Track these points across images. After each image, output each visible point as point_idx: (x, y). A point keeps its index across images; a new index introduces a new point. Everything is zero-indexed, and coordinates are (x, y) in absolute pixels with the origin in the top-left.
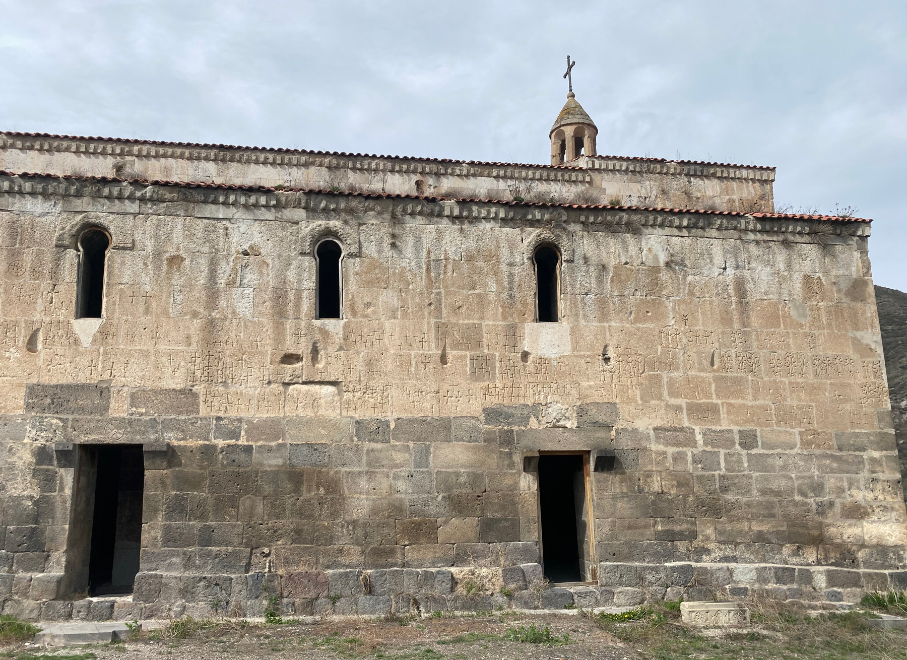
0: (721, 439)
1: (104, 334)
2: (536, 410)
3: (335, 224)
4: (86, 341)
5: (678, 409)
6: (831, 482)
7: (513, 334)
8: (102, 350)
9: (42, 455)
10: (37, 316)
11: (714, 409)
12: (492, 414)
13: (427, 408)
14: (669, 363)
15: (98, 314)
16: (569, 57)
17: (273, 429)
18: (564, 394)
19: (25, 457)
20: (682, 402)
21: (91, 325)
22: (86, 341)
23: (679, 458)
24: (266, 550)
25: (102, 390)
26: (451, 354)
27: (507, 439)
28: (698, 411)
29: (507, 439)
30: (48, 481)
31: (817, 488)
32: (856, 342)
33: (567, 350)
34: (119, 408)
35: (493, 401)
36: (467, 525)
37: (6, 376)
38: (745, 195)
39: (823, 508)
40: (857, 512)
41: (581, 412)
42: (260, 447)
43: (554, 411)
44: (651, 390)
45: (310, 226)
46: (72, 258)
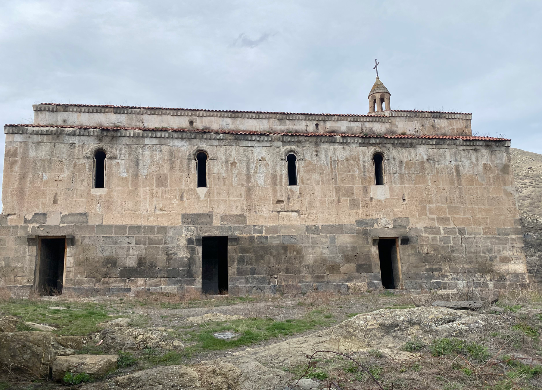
3: (294, 147)
8: (208, 200)
16: (376, 60)
24: (276, 276)
33: (388, 196)
38: (459, 126)
42: (271, 236)
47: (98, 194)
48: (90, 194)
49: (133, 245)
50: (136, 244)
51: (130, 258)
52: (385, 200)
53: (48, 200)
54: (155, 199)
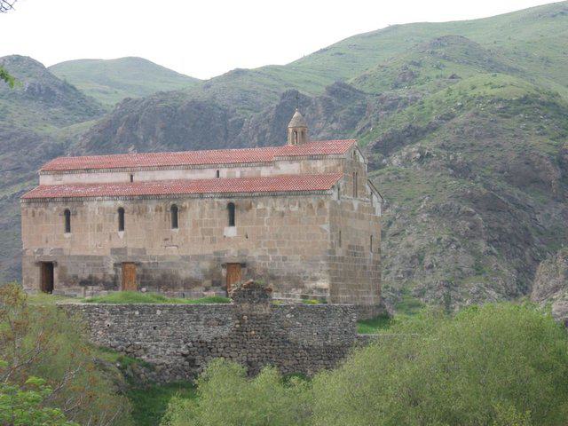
0: (278, 258)
1: (125, 236)
2: (226, 252)
3: (175, 202)
4: (121, 237)
5: (265, 250)
6: (308, 270)
7: (221, 231)
9: (115, 265)
11: (276, 250)
12: (215, 253)
13: (198, 252)
14: (264, 237)
17: (163, 258)
18: (234, 246)
19: (112, 266)
20: (266, 248)
21: (121, 234)
22: (121, 237)
23: (264, 264)
25: (125, 249)
26: (206, 237)
27: (219, 260)
28: (272, 251)
29: (219, 260)
30: (116, 271)
31: (304, 272)
32: (321, 229)
34: (130, 253)
35: (216, 250)
36: (208, 283)
37: (189, 310)
39: (305, 278)
40: (315, 279)
41: (239, 252)
43: (232, 252)
44: (258, 245)
45: (63, 207)
46: (117, 215)
53: (44, 241)
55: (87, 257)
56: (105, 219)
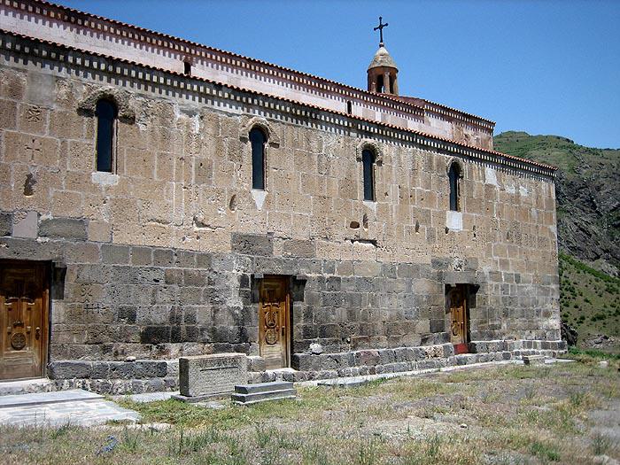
10: (235, 186)
15: (263, 188)
16: (380, 18)
47: (104, 184)
48: (91, 183)
49: (162, 283)
50: (166, 282)
51: (158, 307)
52: (460, 233)
53: (15, 185)
54: (193, 203)
55: (167, 255)
56: (219, 150)
